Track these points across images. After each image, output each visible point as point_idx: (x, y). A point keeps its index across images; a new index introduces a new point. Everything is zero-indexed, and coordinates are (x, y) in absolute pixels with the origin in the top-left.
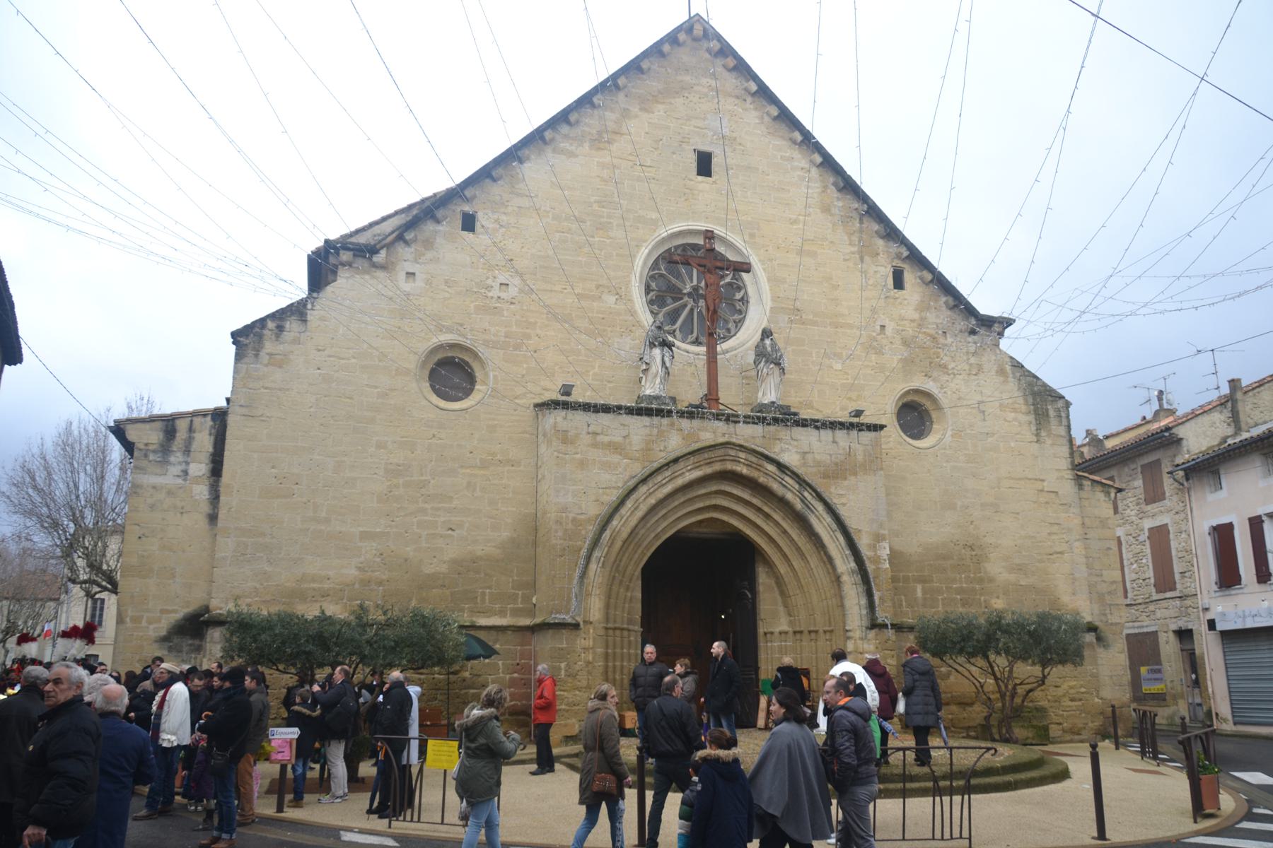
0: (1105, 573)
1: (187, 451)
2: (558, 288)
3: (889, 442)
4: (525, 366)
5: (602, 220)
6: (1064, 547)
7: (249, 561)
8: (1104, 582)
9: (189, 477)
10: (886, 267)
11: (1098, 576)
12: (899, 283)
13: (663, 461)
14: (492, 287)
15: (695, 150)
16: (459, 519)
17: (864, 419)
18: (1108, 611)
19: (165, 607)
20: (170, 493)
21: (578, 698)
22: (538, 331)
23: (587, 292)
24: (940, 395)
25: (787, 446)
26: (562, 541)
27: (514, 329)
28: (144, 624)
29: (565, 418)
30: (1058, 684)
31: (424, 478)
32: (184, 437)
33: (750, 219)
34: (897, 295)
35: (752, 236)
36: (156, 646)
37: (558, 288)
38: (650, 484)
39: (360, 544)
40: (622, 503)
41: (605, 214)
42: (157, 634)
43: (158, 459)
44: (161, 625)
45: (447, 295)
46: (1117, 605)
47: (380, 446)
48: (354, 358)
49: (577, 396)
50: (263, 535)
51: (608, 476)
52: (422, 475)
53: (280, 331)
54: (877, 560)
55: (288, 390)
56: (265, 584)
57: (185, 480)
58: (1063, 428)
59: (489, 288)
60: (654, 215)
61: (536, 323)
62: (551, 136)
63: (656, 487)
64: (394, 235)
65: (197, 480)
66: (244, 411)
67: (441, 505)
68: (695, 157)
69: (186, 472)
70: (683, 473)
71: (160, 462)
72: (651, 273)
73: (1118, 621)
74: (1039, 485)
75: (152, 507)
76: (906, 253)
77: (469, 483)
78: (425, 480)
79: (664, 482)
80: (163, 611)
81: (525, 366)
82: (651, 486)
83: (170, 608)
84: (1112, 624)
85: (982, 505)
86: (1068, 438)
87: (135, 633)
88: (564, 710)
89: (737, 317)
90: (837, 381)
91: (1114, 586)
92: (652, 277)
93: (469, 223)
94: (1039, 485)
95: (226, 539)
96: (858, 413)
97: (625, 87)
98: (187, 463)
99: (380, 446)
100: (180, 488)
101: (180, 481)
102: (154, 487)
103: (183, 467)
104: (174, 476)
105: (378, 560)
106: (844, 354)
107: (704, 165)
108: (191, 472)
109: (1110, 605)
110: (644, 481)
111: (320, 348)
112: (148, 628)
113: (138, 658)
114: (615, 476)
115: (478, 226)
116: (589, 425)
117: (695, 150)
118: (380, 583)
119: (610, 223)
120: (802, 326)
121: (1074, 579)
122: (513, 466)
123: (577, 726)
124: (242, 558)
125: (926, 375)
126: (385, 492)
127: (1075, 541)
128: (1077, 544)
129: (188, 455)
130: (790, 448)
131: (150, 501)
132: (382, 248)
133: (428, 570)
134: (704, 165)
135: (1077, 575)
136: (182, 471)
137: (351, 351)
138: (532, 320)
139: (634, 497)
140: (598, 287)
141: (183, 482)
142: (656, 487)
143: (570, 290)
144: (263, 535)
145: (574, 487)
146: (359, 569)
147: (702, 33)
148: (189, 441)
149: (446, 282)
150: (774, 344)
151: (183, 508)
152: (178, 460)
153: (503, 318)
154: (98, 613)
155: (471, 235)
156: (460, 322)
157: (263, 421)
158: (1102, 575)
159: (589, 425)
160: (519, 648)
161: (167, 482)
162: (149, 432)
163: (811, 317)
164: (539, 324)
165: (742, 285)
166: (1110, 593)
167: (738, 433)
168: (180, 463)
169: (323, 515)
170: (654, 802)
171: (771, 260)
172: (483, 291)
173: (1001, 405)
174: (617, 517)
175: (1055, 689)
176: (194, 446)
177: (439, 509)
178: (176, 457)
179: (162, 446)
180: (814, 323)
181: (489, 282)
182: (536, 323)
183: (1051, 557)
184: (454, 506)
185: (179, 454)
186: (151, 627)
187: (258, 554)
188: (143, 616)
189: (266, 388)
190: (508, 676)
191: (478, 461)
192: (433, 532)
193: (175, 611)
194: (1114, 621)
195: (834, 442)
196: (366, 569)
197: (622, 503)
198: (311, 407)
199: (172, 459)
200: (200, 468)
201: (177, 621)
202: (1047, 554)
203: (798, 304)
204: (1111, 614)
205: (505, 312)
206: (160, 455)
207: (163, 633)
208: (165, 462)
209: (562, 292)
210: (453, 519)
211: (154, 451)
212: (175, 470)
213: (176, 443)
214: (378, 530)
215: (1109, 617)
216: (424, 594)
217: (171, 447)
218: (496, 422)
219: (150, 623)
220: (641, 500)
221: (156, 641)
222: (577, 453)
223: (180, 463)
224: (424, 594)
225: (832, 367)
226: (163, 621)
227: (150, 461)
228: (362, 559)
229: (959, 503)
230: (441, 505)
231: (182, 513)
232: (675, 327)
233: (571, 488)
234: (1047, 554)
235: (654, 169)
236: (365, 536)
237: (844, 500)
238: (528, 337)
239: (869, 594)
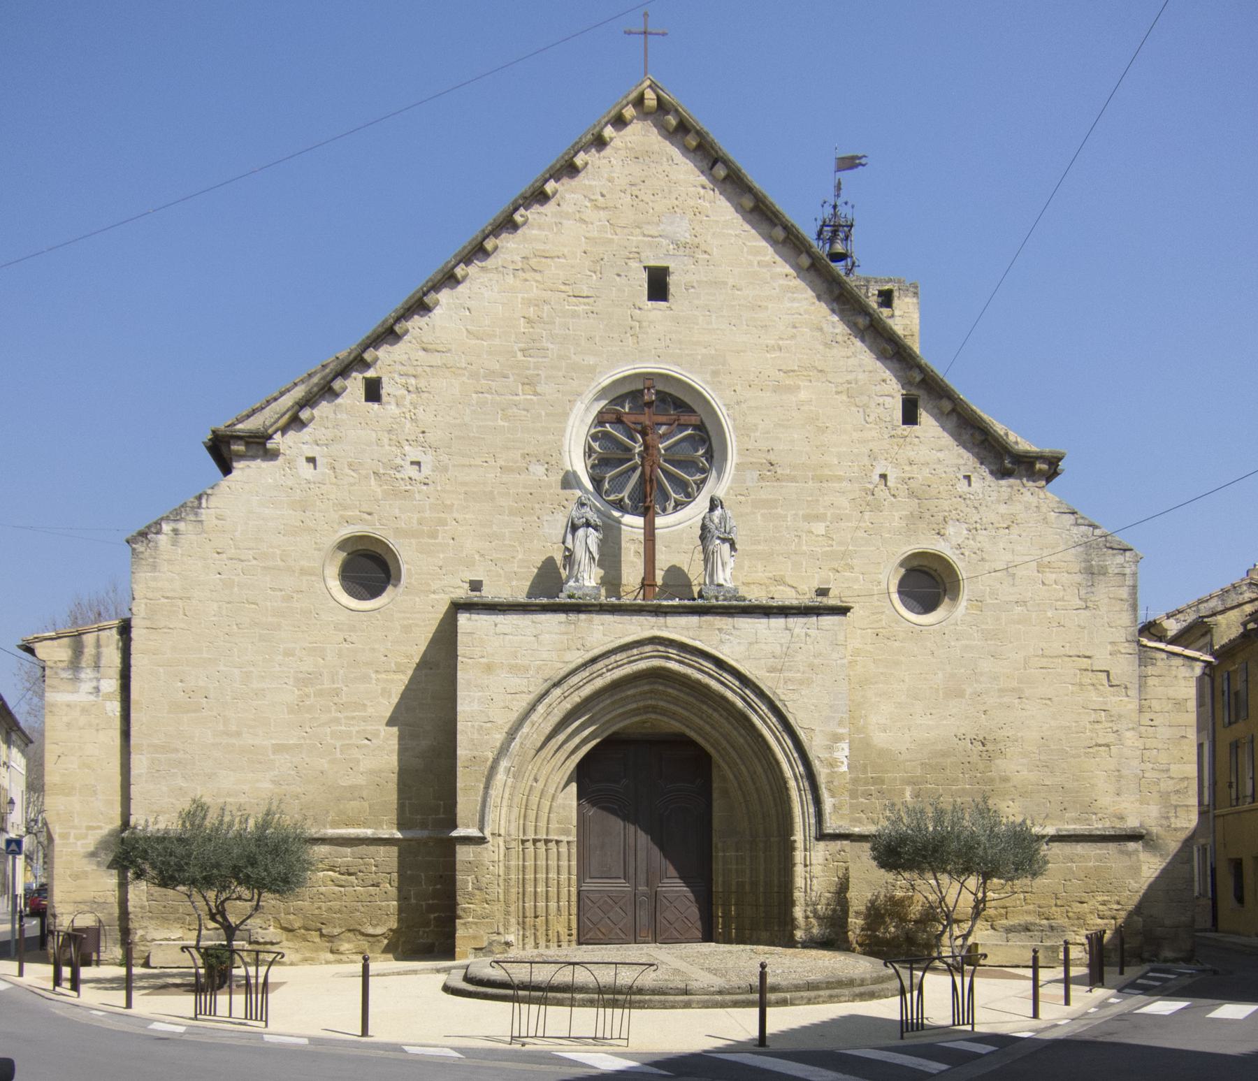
0: (1172, 767)
1: (97, 667)
2: (478, 461)
3: (881, 620)
4: (441, 556)
5: (528, 372)
6: (1111, 738)
7: (164, 777)
8: (1172, 778)
9: (101, 694)
10: (893, 397)
11: (1163, 771)
12: (910, 417)
13: (580, 661)
14: (402, 467)
15: (645, 268)
16: (374, 728)
17: (831, 601)
18: (1172, 814)
19: (91, 824)
20: (85, 711)
21: (487, 911)
22: (455, 515)
23: (511, 464)
24: (954, 558)
25: (728, 637)
26: (468, 752)
27: (427, 514)
28: (72, 840)
29: (469, 619)
30: (1083, 900)
31: (335, 686)
32: (93, 653)
33: (713, 352)
34: (905, 433)
35: (715, 373)
36: (85, 861)
37: (478, 461)
38: (565, 686)
39: (272, 757)
40: (532, 708)
41: (532, 365)
42: (85, 850)
43: (70, 677)
44: (89, 842)
45: (352, 480)
46: (1187, 806)
47: (288, 653)
48: (255, 559)
49: (490, 593)
50: (177, 750)
51: (518, 681)
52: (334, 683)
53: (176, 534)
54: (832, 764)
55: (189, 598)
56: (182, 800)
57: (97, 696)
58: (1126, 589)
59: (398, 468)
60: (591, 360)
61: (453, 505)
62: (463, 273)
63: (572, 690)
64: (287, 416)
65: (108, 697)
66: (148, 624)
67: (355, 714)
68: (645, 276)
69: (97, 689)
70: (603, 673)
71: (71, 679)
72: (593, 431)
73: (1185, 826)
74: (1085, 663)
75: (68, 725)
76: (918, 378)
77: (384, 690)
78: (338, 688)
79: (581, 684)
80: (90, 828)
81: (441, 556)
82: (566, 689)
83: (95, 825)
84: (1175, 830)
85: (1000, 690)
86: (1131, 601)
87: (65, 850)
88: (472, 923)
89: (698, 477)
90: (818, 549)
91: (1185, 784)
92: (595, 437)
93: (373, 391)
94: (1085, 663)
95: (140, 756)
96: (823, 592)
97: (555, 193)
98: (98, 680)
99: (288, 653)
100: (94, 705)
101: (92, 698)
102: (68, 706)
103: (94, 684)
104: (87, 693)
105: (293, 773)
106: (829, 515)
107: (658, 285)
108: (102, 688)
109: (1176, 807)
110: (557, 684)
111: (219, 550)
112: (76, 843)
113: (68, 872)
114: (526, 680)
115: (383, 392)
116: (496, 625)
117: (645, 268)
118: (297, 797)
119: (538, 375)
120: (775, 484)
121: (1120, 777)
122: (431, 669)
123: (485, 938)
124: (156, 775)
125: (938, 534)
126: (296, 702)
127: (1128, 730)
128: (1129, 734)
129: (98, 672)
130: (732, 638)
131: (65, 719)
132: (275, 432)
133: (345, 782)
134: (658, 285)
135: (1125, 772)
136: (94, 688)
137: (250, 552)
138: (448, 502)
139: (547, 701)
140: (524, 456)
141: (95, 699)
142: (572, 690)
143: (492, 462)
144: (177, 750)
145: (480, 694)
146: (273, 782)
147: (655, 102)
148: (98, 656)
149: (350, 465)
150: (723, 519)
151: (98, 725)
152: (88, 677)
153: (415, 502)
154: (728, 998)
155: (376, 406)
156: (369, 510)
157: (165, 633)
158: (1168, 770)
159: (496, 625)
160: (442, 859)
161: (82, 700)
162: (58, 649)
163: (788, 471)
164: (455, 506)
165: (705, 436)
166: (1177, 792)
167: (669, 625)
168: (91, 680)
169: (234, 728)
170: (719, 1059)
171: (738, 403)
172: (392, 472)
173: (1039, 565)
174: (527, 724)
175: (1079, 905)
176: (103, 662)
177: (353, 718)
178: (87, 674)
179: (71, 662)
180: (793, 479)
181: (399, 461)
182: (453, 505)
183: (1091, 750)
184: (369, 715)
185: (88, 671)
186: (79, 843)
187: (172, 771)
188: (69, 833)
189: (167, 598)
190: (431, 888)
191: (393, 665)
192: (347, 742)
193: (100, 828)
194: (1179, 825)
195: (787, 629)
196: (281, 782)
197: (532, 708)
198: (215, 615)
199: (83, 676)
200: (111, 685)
201: (102, 837)
202: (1084, 748)
203: (772, 457)
204: (1176, 817)
205: (417, 496)
206: (70, 672)
207: (92, 849)
208: (76, 679)
209: (482, 466)
210: (369, 728)
211: (63, 669)
212: (87, 687)
213: (85, 659)
214: (291, 742)
215: (1173, 820)
216: (341, 807)
217: (80, 663)
218: (411, 621)
219: (77, 839)
220: (554, 705)
221: (85, 857)
222: (483, 657)
223: (91, 680)
224: (341, 807)
225: (812, 533)
226: (90, 837)
227: (62, 679)
228: (276, 773)
229: (969, 691)
230: (355, 714)
231: (97, 730)
232: (621, 496)
233: (477, 694)
234: (1084, 748)
235: (592, 300)
236: (279, 749)
237: (795, 696)
238: (443, 522)
239: (818, 802)
